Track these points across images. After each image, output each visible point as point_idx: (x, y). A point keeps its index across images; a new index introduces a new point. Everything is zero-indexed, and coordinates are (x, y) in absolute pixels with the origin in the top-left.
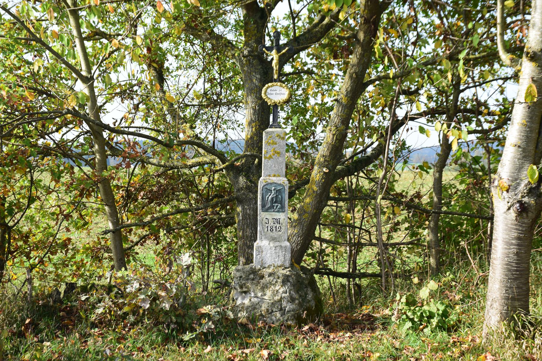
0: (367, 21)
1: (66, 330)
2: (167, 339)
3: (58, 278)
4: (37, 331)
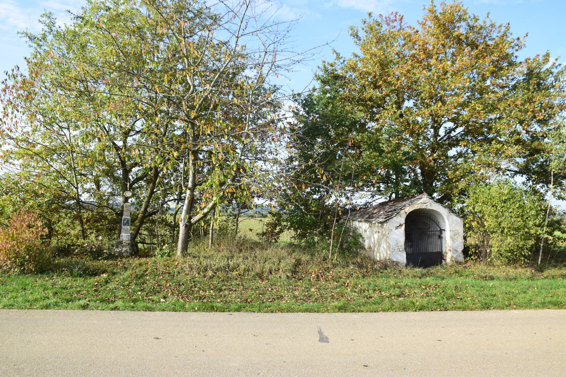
0: (155, 175)
1: (68, 256)
2: (94, 259)
3: (66, 243)
4: (59, 256)
